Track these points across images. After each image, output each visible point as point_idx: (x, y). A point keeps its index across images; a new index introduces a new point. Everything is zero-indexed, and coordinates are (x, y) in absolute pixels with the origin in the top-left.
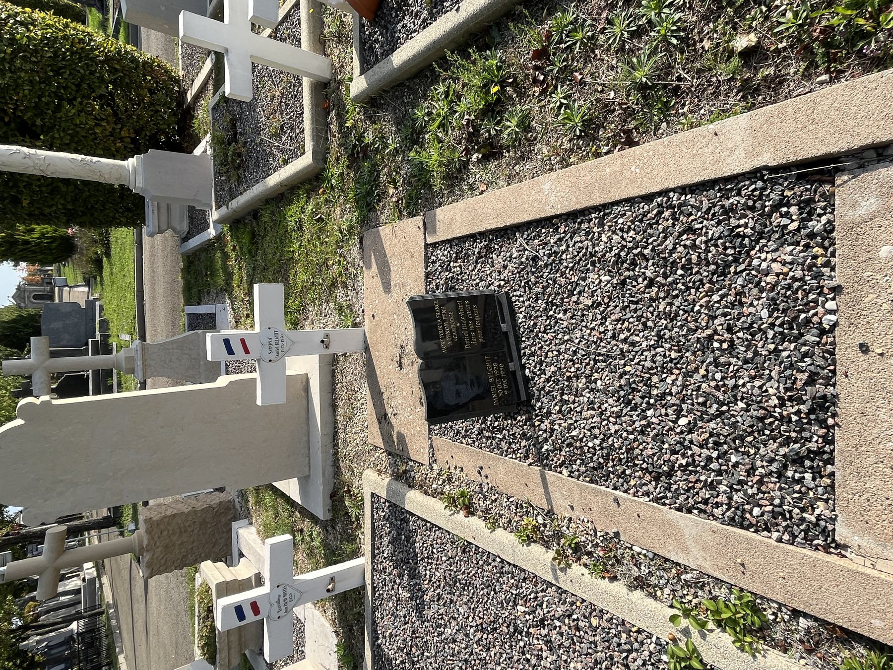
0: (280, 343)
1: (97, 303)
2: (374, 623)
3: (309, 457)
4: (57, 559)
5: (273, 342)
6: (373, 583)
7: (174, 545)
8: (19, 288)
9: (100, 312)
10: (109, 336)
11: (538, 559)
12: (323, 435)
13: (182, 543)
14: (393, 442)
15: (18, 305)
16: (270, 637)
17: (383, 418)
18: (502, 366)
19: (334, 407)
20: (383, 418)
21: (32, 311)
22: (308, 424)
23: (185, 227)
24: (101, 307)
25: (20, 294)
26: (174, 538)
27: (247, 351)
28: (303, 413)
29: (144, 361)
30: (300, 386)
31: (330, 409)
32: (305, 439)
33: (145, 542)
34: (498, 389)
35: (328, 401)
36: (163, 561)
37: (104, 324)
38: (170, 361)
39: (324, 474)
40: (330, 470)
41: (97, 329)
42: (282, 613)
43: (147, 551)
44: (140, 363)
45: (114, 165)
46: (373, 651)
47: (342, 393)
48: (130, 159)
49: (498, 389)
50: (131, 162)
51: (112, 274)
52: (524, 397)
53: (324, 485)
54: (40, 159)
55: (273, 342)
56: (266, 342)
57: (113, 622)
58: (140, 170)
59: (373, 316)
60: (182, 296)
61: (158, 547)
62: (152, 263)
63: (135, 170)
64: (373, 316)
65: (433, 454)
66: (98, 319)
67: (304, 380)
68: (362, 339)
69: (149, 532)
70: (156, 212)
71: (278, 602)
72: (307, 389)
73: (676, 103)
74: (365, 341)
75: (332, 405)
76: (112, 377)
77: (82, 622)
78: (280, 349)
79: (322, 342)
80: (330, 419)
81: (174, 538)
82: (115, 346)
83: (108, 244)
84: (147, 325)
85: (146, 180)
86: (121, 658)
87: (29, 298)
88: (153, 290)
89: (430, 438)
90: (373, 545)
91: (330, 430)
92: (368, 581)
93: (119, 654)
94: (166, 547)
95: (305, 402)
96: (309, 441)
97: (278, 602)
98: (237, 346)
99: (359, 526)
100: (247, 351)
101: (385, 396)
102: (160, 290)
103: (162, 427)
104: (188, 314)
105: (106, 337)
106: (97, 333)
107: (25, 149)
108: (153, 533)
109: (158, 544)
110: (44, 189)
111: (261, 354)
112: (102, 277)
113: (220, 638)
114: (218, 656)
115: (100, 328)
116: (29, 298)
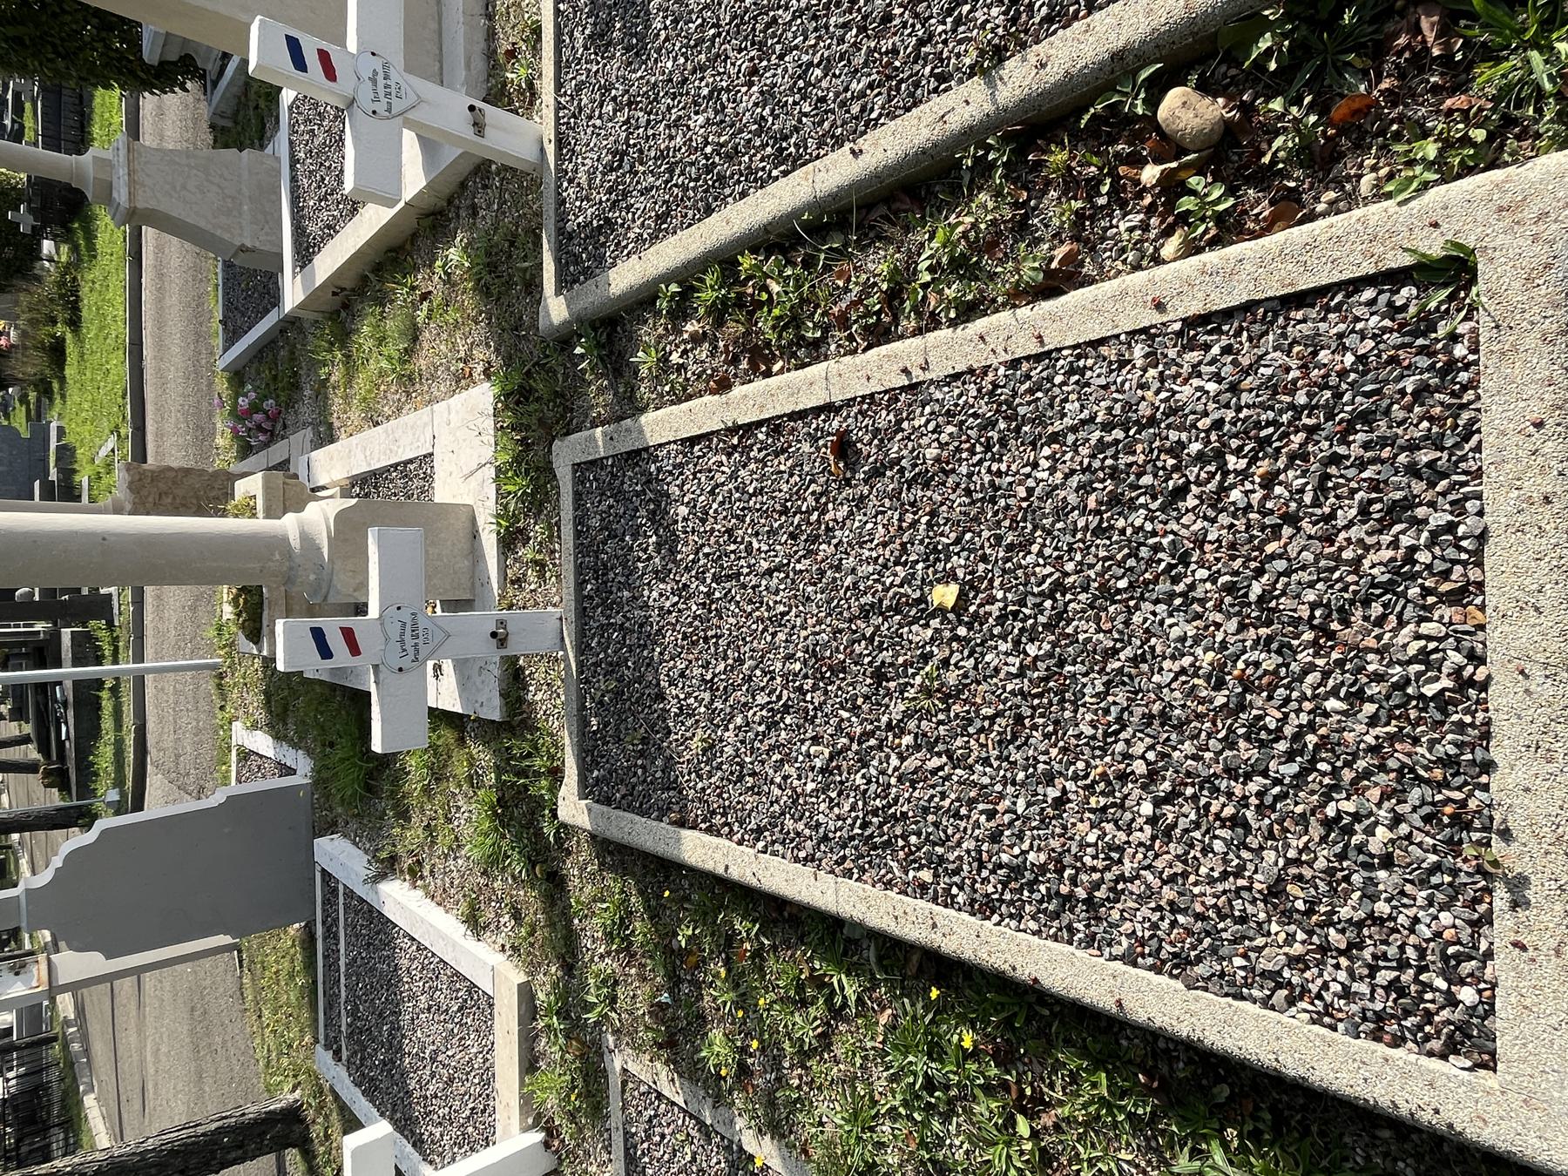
3: (441, 62)
10: (74, 471)
16: (354, 138)
29: (131, 173)
38: (184, 187)
41: (52, 464)
44: (122, 172)
46: (557, 260)
51: (82, 355)
57: (76, 1047)
60: (208, 227)
62: (159, 300)
71: (374, 81)
72: (475, 535)
73: (1385, 1142)
79: (494, 635)
83: (76, 302)
86: (89, 1101)
88: (160, 324)
93: (86, 1092)
98: (336, 642)
100: (355, 650)
105: (68, 473)
108: (144, 492)
111: (355, 90)
112: (62, 380)
115: (57, 460)
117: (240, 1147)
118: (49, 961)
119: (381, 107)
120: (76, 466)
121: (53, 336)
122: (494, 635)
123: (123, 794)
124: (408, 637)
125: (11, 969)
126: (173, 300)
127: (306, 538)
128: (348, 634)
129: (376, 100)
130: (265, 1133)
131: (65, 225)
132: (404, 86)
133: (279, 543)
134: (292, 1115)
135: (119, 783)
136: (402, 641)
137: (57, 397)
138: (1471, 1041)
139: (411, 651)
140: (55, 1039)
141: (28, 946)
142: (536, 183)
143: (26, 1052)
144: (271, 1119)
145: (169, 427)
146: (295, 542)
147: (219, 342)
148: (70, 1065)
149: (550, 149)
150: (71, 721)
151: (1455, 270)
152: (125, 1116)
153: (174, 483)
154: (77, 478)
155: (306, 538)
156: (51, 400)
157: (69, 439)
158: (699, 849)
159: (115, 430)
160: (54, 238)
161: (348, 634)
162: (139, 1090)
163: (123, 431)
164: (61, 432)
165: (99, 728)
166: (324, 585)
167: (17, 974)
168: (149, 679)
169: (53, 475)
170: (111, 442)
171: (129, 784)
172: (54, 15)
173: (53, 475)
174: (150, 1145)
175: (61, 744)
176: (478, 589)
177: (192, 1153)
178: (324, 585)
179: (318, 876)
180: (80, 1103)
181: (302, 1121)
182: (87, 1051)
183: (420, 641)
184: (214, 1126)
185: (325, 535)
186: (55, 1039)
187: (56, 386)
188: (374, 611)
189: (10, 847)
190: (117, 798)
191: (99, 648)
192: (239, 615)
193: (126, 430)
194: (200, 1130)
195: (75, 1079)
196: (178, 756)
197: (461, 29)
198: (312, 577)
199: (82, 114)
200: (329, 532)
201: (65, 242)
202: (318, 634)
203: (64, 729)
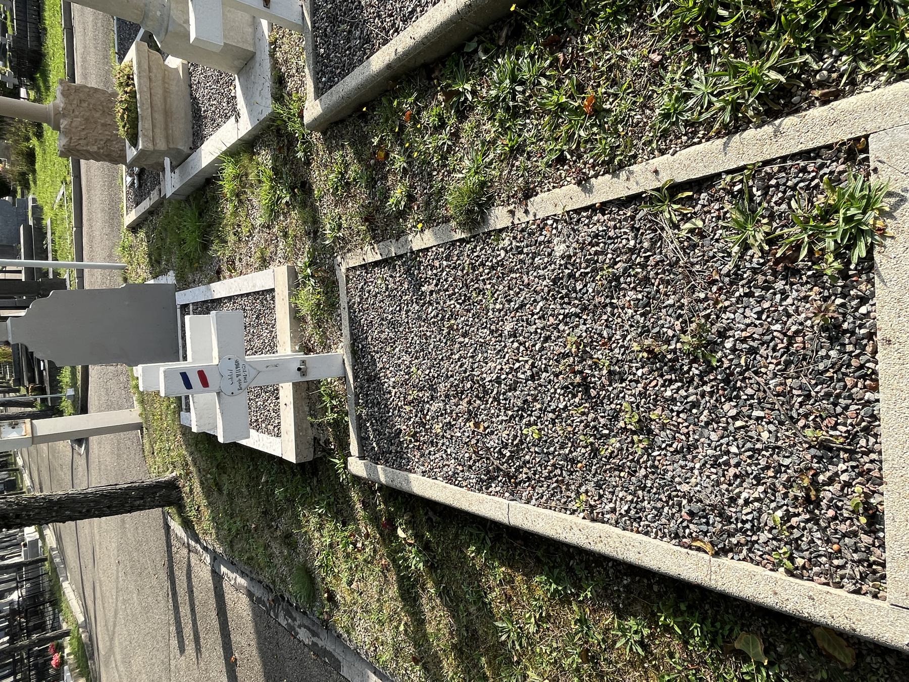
57: (58, 560)
79: (299, 369)
86: (65, 585)
93: (63, 581)
108: (71, 98)
114: (140, 124)
117: (142, 498)
118: (32, 423)
121: (28, 148)
123: (76, 390)
125: (10, 425)
126: (92, 59)
130: (156, 493)
131: (33, 79)
134: (172, 485)
135: (74, 385)
137: (32, 184)
140: (45, 560)
143: (30, 567)
144: (159, 486)
148: (54, 569)
152: (84, 578)
153: (89, 95)
156: (28, 188)
158: (422, 485)
159: (64, 181)
160: (26, 86)
162: (90, 552)
163: (68, 179)
164: (34, 200)
166: (166, 19)
167: (13, 428)
168: (86, 271)
171: (79, 383)
174: (89, 490)
175: (41, 373)
177: (114, 498)
178: (166, 19)
180: (60, 587)
181: (178, 487)
182: (64, 561)
184: (126, 486)
186: (45, 560)
187: (31, 177)
189: (18, 470)
190: (73, 393)
193: (70, 178)
194: (118, 487)
195: (57, 575)
198: (159, 13)
199: (39, 7)
201: (32, 89)
203: (42, 364)
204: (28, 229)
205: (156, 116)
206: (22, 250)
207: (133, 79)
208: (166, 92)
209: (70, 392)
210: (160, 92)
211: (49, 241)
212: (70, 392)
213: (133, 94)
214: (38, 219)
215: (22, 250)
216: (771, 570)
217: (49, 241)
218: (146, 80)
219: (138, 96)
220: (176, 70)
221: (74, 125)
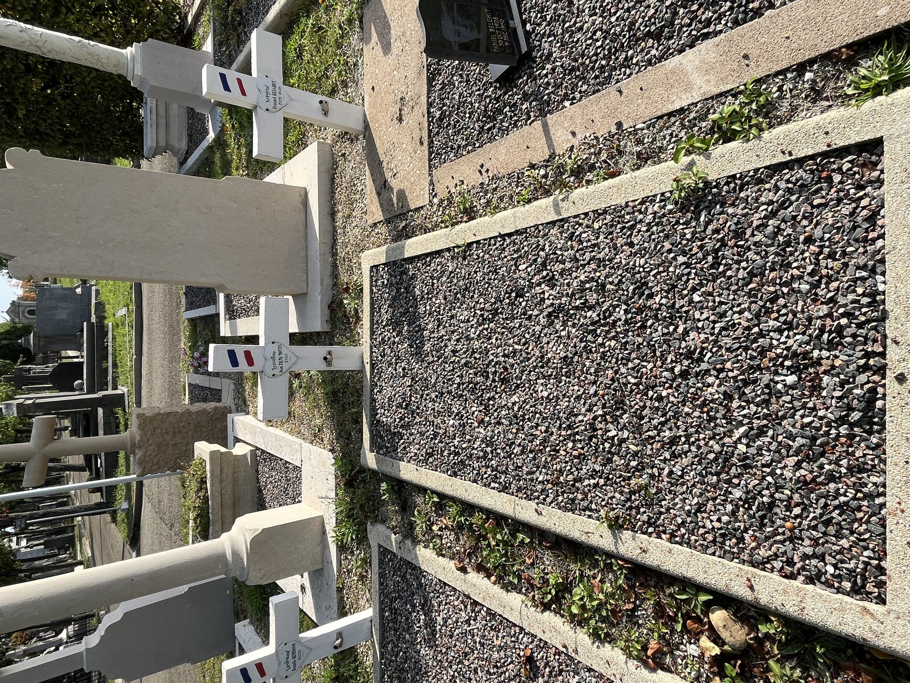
0: (278, 95)
1: (94, 288)
2: (374, 400)
3: (307, 273)
4: (45, 445)
5: (270, 91)
6: (371, 360)
7: (167, 444)
8: (13, 303)
9: (96, 297)
10: (105, 318)
11: (541, 211)
12: (322, 243)
13: (175, 445)
14: (393, 205)
15: (12, 320)
17: (383, 187)
18: (502, 22)
19: (333, 214)
20: (383, 187)
21: (25, 321)
22: (306, 240)
23: (183, 145)
24: (97, 291)
25: (14, 309)
26: (168, 438)
27: (244, 93)
28: (301, 227)
30: (297, 199)
31: (329, 218)
32: (303, 254)
33: (138, 438)
34: (498, 40)
35: (327, 210)
36: (155, 460)
37: (100, 306)
39: (322, 284)
40: (328, 281)
42: (277, 372)
43: (140, 447)
45: (112, 51)
46: (371, 431)
47: (343, 182)
48: (129, 48)
49: (498, 40)
50: (129, 51)
52: (524, 49)
53: (322, 293)
54: (36, 35)
55: (270, 91)
56: (264, 89)
58: (139, 58)
59: (373, 88)
61: (150, 445)
63: (133, 57)
64: (373, 88)
65: (433, 190)
66: (93, 301)
67: (303, 194)
68: (362, 118)
69: (141, 427)
70: (154, 127)
71: (273, 358)
72: (324, 532)
74: (365, 115)
75: (331, 213)
76: (107, 360)
77: (71, 628)
78: (277, 100)
79: (325, 358)
80: (330, 228)
81: (168, 438)
82: (110, 327)
84: (145, 329)
85: (144, 68)
87: (23, 313)
89: (430, 175)
90: (372, 320)
91: (329, 239)
92: (367, 359)
94: (159, 446)
95: (303, 216)
96: (307, 255)
97: (273, 358)
99: (358, 319)
100: (244, 93)
101: (385, 164)
102: (156, 316)
103: (156, 207)
104: (189, 320)
106: (93, 316)
107: (22, 24)
108: (146, 429)
109: (150, 441)
110: (40, 99)
111: (258, 100)
113: (214, 510)
114: (211, 528)
116: (23, 313)
119: (277, 372)
120: (106, 315)
122: (325, 358)
124: (291, 660)
127: (235, 554)
128: (248, 355)
129: (275, 368)
132: (289, 354)
133: (218, 560)
135: (128, 498)
136: (287, 662)
138: (868, 583)
139: (292, 666)
140: (93, 616)
141: (79, 558)
142: (359, 393)
145: (155, 326)
146: (229, 557)
147: (183, 309)
149: (368, 367)
150: (103, 458)
151: (875, 146)
154: (106, 322)
155: (235, 554)
157: (103, 298)
161: (248, 355)
165: (117, 461)
169: (93, 319)
170: (124, 311)
171: (134, 501)
172: (98, 132)
173: (93, 319)
176: (326, 563)
179: (237, 645)
183: (297, 659)
185: (245, 551)
186: (93, 616)
188: (262, 342)
190: (127, 507)
191: (117, 418)
192: (197, 527)
193: (133, 307)
196: (159, 502)
197: (318, 264)
200: (247, 553)
202: (223, 77)
204: (91, 325)
205: (226, 513)
206: (85, 345)
207: (205, 482)
208: (235, 481)
209: (125, 505)
210: (230, 488)
211: (110, 340)
212: (125, 505)
213: (206, 499)
214: (101, 318)
215: (85, 345)
216: (720, 557)
217: (110, 340)
218: (218, 485)
219: (210, 503)
220: (245, 456)
221: (147, 454)
